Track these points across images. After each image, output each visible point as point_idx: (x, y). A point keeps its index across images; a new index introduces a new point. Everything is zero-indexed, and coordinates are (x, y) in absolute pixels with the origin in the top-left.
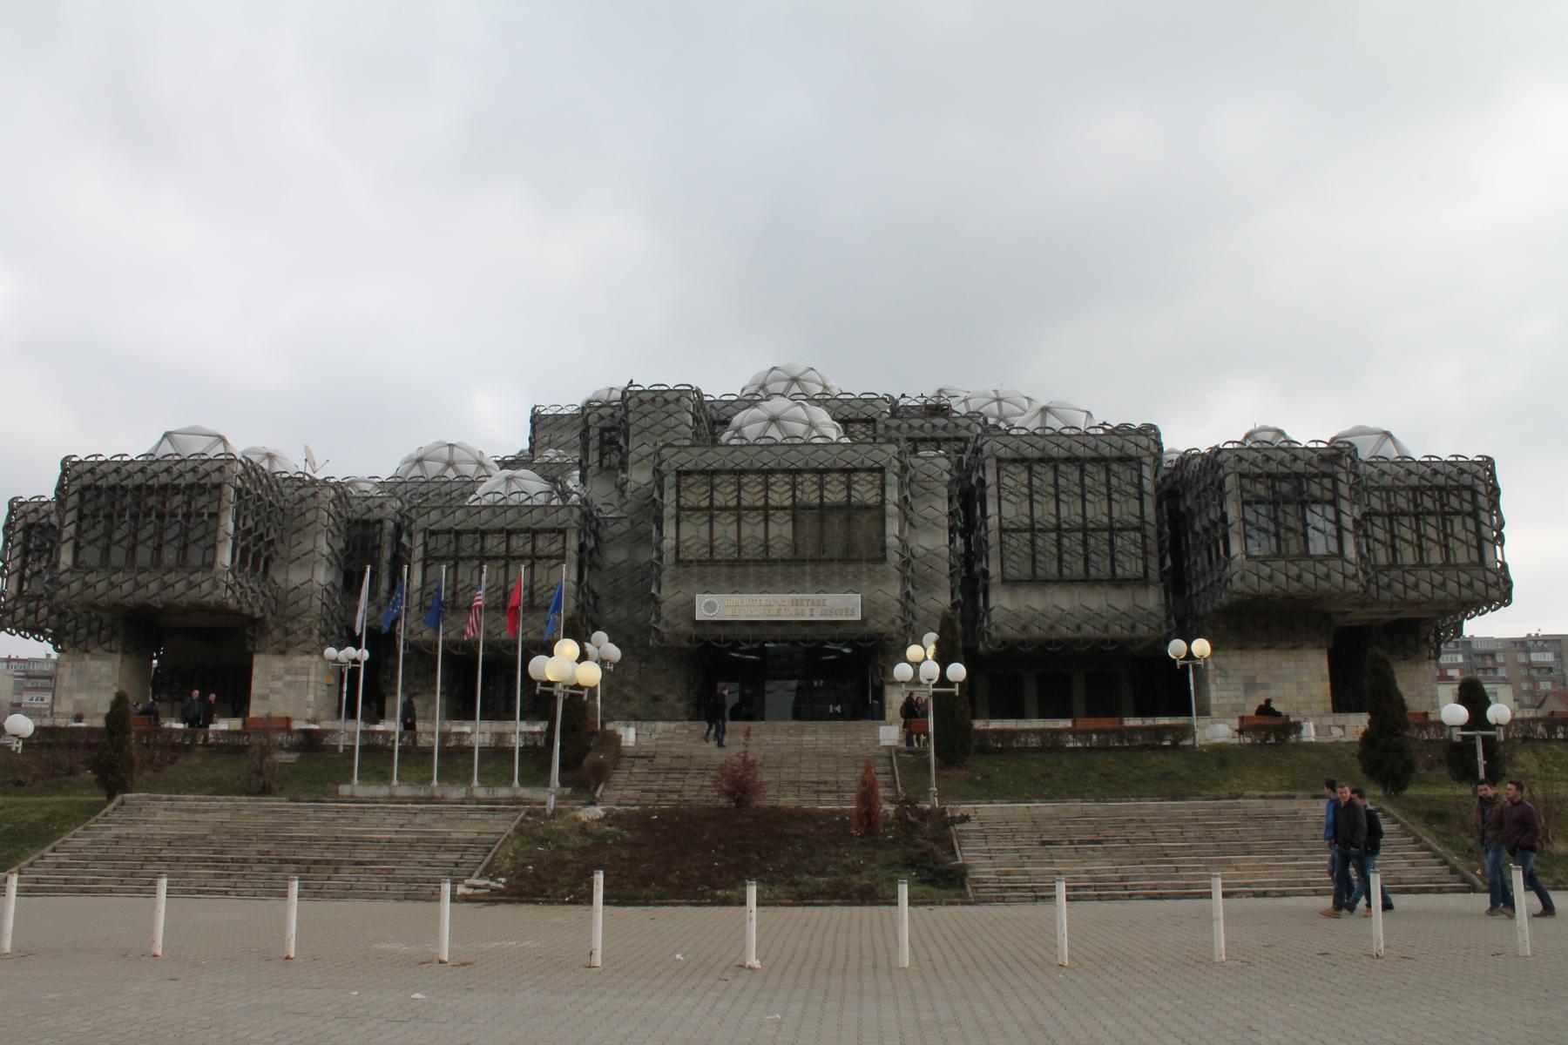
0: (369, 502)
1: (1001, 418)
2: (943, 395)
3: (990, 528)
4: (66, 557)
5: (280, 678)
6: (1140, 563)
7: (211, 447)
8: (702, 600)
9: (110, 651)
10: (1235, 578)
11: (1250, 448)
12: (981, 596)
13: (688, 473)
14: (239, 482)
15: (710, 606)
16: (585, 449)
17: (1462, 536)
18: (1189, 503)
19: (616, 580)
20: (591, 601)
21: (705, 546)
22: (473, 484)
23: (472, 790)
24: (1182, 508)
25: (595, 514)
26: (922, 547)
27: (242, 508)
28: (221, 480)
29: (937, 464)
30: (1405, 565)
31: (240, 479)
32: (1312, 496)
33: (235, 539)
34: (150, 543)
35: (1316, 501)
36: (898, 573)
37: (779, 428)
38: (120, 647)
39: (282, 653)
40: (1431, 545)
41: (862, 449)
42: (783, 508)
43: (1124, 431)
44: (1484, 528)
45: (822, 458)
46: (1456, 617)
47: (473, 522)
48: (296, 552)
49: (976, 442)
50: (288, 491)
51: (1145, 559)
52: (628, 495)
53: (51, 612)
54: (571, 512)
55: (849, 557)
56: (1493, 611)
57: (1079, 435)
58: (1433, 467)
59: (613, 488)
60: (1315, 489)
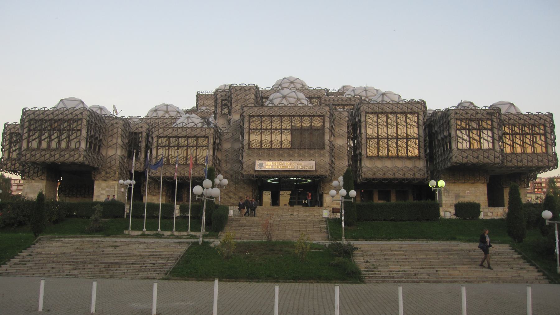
0: (137, 126)
1: (367, 97)
2: (345, 88)
3: (362, 137)
4: (24, 145)
5: (104, 190)
6: (417, 151)
7: (78, 105)
8: (257, 162)
9: (42, 179)
10: (453, 157)
11: (460, 109)
12: (359, 162)
13: (253, 116)
14: (88, 118)
15: (261, 165)
16: (216, 107)
17: (540, 143)
18: (436, 129)
19: (227, 155)
20: (218, 163)
21: (259, 143)
22: (175, 119)
23: (173, 232)
24: (433, 131)
25: (219, 131)
26: (338, 144)
27: (90, 128)
28: (82, 117)
29: (343, 114)
30: (517, 153)
31: (89, 117)
32: (483, 127)
33: (87, 139)
34: (56, 140)
35: (485, 129)
36: (329, 153)
37: (286, 100)
38: (45, 178)
39: (105, 180)
40: (527, 146)
41: (316, 109)
42: (287, 129)
43: (412, 102)
44: (548, 140)
45: (302, 112)
46: (535, 173)
47: (175, 133)
48: (110, 143)
49: (358, 106)
50: (107, 121)
51: (419, 150)
52: (231, 124)
53: (20, 164)
54: (211, 130)
55: (311, 147)
56: (550, 171)
57: (396, 104)
58: (529, 116)
59: (226, 121)
60: (485, 125)
